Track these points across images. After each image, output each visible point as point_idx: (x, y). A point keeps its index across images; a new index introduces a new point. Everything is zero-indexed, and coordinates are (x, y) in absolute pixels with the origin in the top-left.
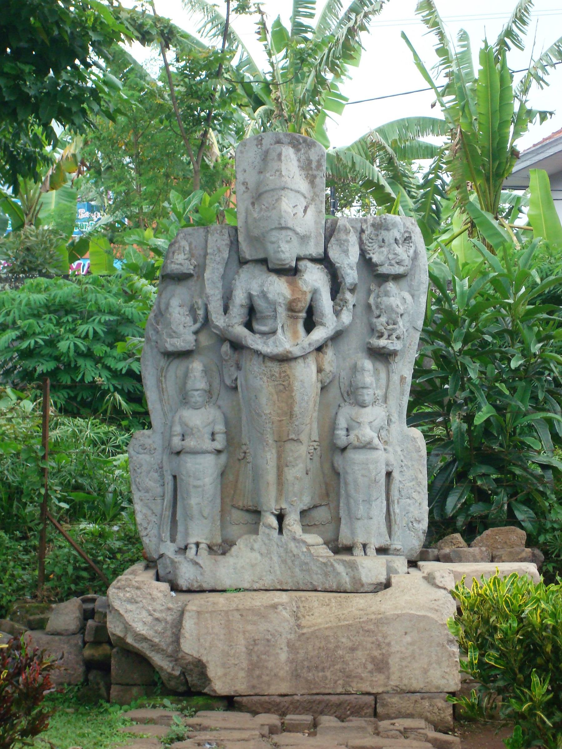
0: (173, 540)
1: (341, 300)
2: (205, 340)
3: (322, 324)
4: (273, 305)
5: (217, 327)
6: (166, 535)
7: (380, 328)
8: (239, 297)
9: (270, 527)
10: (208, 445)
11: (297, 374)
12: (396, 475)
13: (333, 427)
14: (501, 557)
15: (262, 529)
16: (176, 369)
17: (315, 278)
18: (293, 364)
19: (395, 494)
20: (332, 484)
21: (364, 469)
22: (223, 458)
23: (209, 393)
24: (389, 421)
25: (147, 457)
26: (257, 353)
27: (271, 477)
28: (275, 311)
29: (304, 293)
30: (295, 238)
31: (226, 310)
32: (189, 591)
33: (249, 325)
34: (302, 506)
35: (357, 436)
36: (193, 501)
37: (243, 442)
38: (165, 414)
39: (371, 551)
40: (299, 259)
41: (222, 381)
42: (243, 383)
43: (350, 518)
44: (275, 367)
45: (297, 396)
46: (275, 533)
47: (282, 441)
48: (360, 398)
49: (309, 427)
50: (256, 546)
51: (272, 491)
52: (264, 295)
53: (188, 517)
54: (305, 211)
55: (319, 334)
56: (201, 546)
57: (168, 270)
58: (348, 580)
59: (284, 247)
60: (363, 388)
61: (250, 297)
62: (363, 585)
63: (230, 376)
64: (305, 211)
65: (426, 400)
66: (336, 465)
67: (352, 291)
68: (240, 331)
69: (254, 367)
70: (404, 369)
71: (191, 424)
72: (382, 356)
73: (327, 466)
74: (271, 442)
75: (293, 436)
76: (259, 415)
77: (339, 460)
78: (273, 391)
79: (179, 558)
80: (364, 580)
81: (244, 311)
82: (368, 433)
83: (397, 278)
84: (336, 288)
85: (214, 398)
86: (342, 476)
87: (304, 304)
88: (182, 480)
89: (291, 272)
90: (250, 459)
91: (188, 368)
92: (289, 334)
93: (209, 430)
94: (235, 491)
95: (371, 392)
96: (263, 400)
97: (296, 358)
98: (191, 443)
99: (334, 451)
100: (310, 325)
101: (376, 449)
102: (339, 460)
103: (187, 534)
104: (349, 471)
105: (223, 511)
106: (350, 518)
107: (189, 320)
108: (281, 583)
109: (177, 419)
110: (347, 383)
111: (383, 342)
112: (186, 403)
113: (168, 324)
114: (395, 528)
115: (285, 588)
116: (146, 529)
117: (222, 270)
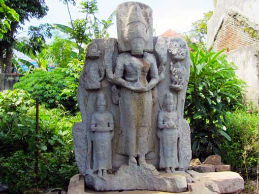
0: (92, 168)
1: (161, 68)
2: (105, 84)
3: (155, 78)
4: (135, 69)
5: (110, 79)
6: (89, 166)
7: (176, 80)
8: (120, 66)
9: (134, 162)
10: (107, 129)
11: (145, 98)
12: (181, 138)
13: (157, 120)
14: (219, 169)
15: (130, 163)
16: (92, 96)
17: (151, 59)
18: (144, 94)
19: (180, 146)
20: (157, 143)
21: (169, 137)
22: (113, 133)
23: (107, 106)
24: (178, 117)
25: (80, 133)
26: (129, 89)
27: (134, 142)
28: (137, 72)
29: (148, 65)
30: (143, 42)
31: (114, 72)
32: (100, 191)
33: (124, 78)
34: (145, 153)
35: (168, 124)
36: (101, 152)
37: (121, 126)
38: (87, 115)
39: (173, 170)
40: (144, 51)
41: (112, 101)
42: (122, 102)
43: (164, 157)
44: (137, 96)
45: (146, 108)
46: (136, 165)
47: (138, 127)
48: (168, 108)
49: (148, 121)
50: (128, 171)
51: (135, 147)
52: (131, 65)
53: (98, 158)
54: (146, 31)
55: (154, 82)
56: (104, 171)
57: (89, 55)
58: (171, 187)
59: (139, 45)
60: (170, 104)
61: (125, 66)
62: (178, 190)
63: (116, 100)
64: (146, 31)
65: (189, 111)
66: (158, 135)
67: (165, 65)
68: (121, 80)
69: (128, 95)
70: (183, 96)
71: (100, 120)
72: (176, 91)
73: (154, 136)
74: (134, 127)
75: (143, 125)
76: (129, 116)
77: (160, 134)
78: (136, 106)
79: (95, 176)
80: (179, 187)
81: (122, 72)
82: (172, 123)
83: (181, 60)
84: (159, 64)
85: (109, 108)
86: (161, 140)
87: (147, 70)
88: (95, 143)
89: (141, 57)
90: (124, 134)
91: (98, 96)
92: (142, 81)
93: (107, 122)
94: (117, 147)
95: (172, 105)
96: (131, 110)
97: (145, 92)
98: (99, 128)
99: (158, 129)
100: (149, 78)
101: (175, 129)
102: (160, 134)
103: (98, 166)
104: (165, 138)
105: (112, 156)
106: (164, 157)
107: (98, 75)
108: (139, 187)
109: (93, 117)
110: (162, 102)
111: (177, 86)
112: (97, 111)
113: (89, 78)
114: (180, 159)
115: (142, 189)
116: (80, 163)
117: (112, 56)
